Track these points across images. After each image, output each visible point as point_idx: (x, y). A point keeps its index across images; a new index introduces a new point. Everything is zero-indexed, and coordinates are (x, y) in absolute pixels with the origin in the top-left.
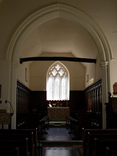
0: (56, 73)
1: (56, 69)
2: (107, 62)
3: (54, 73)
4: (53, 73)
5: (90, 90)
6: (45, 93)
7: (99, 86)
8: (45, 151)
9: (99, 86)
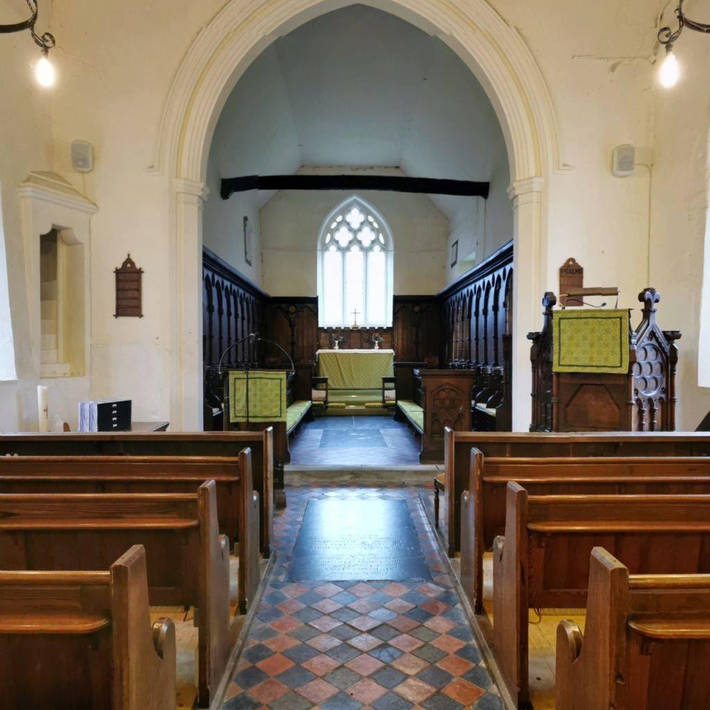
0: (350, 236)
1: (350, 230)
2: (541, 180)
3: (343, 236)
4: (337, 236)
5: (465, 291)
6: (310, 304)
7: (489, 282)
8: (308, 505)
9: (489, 282)
